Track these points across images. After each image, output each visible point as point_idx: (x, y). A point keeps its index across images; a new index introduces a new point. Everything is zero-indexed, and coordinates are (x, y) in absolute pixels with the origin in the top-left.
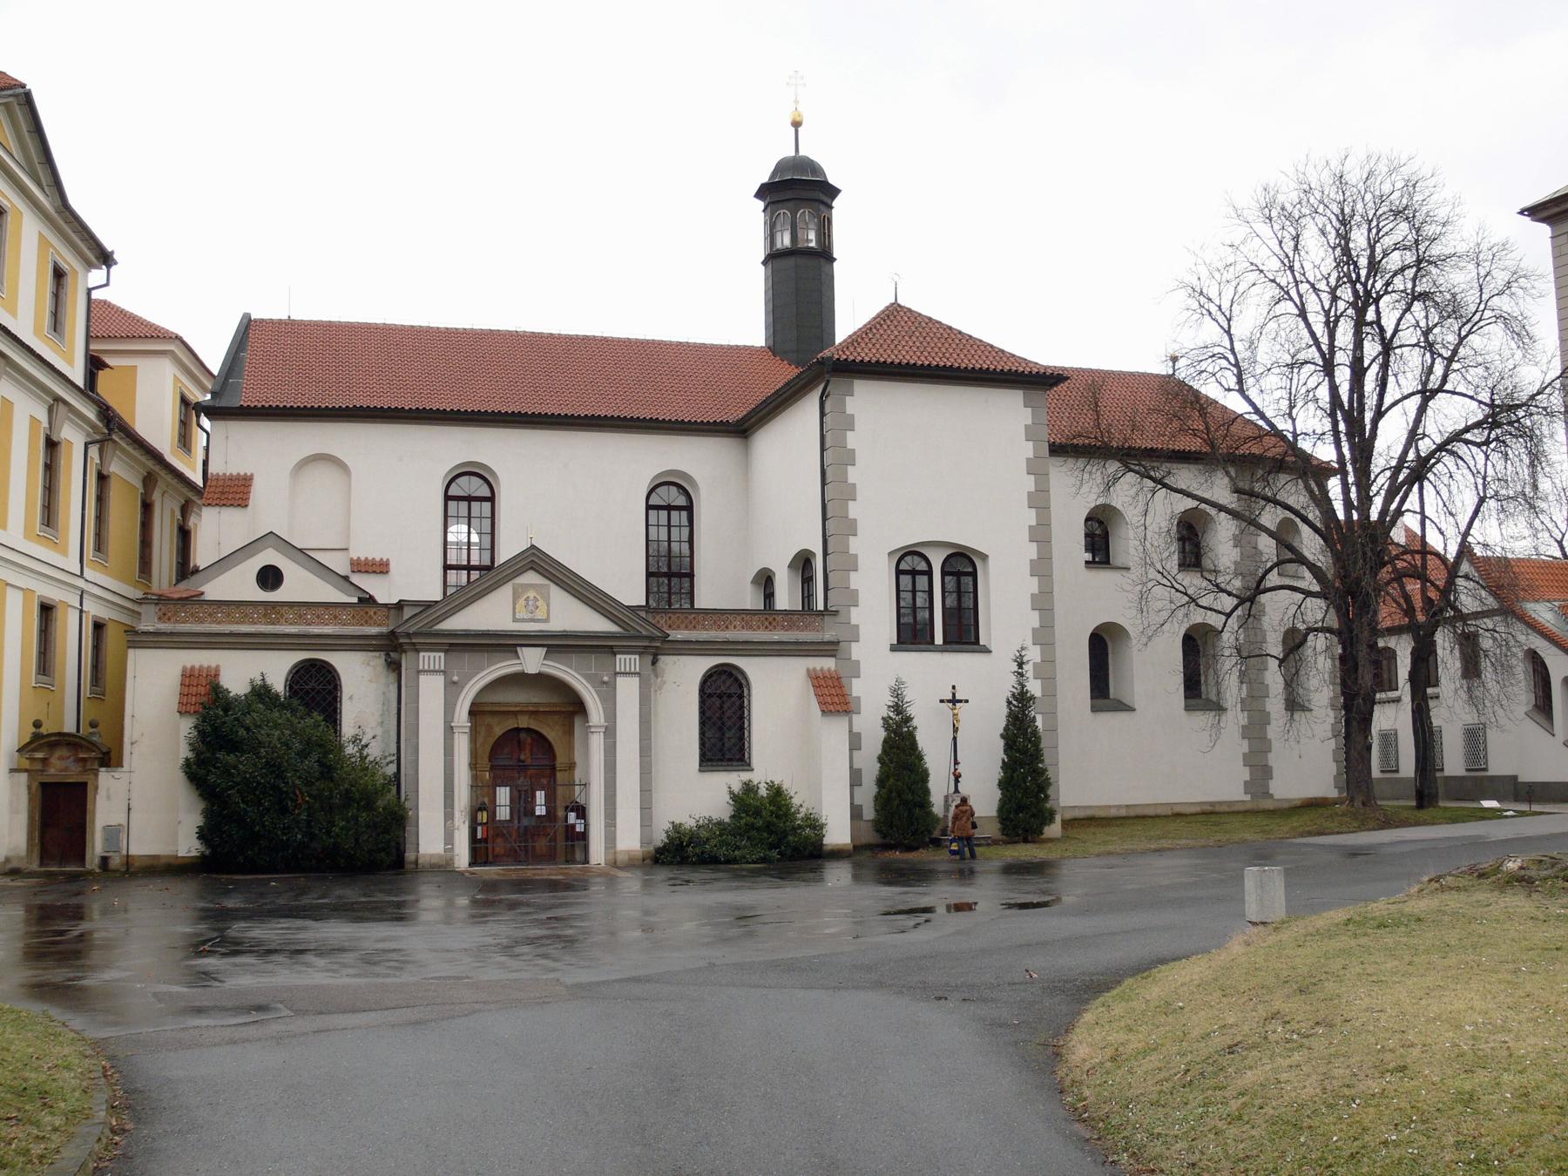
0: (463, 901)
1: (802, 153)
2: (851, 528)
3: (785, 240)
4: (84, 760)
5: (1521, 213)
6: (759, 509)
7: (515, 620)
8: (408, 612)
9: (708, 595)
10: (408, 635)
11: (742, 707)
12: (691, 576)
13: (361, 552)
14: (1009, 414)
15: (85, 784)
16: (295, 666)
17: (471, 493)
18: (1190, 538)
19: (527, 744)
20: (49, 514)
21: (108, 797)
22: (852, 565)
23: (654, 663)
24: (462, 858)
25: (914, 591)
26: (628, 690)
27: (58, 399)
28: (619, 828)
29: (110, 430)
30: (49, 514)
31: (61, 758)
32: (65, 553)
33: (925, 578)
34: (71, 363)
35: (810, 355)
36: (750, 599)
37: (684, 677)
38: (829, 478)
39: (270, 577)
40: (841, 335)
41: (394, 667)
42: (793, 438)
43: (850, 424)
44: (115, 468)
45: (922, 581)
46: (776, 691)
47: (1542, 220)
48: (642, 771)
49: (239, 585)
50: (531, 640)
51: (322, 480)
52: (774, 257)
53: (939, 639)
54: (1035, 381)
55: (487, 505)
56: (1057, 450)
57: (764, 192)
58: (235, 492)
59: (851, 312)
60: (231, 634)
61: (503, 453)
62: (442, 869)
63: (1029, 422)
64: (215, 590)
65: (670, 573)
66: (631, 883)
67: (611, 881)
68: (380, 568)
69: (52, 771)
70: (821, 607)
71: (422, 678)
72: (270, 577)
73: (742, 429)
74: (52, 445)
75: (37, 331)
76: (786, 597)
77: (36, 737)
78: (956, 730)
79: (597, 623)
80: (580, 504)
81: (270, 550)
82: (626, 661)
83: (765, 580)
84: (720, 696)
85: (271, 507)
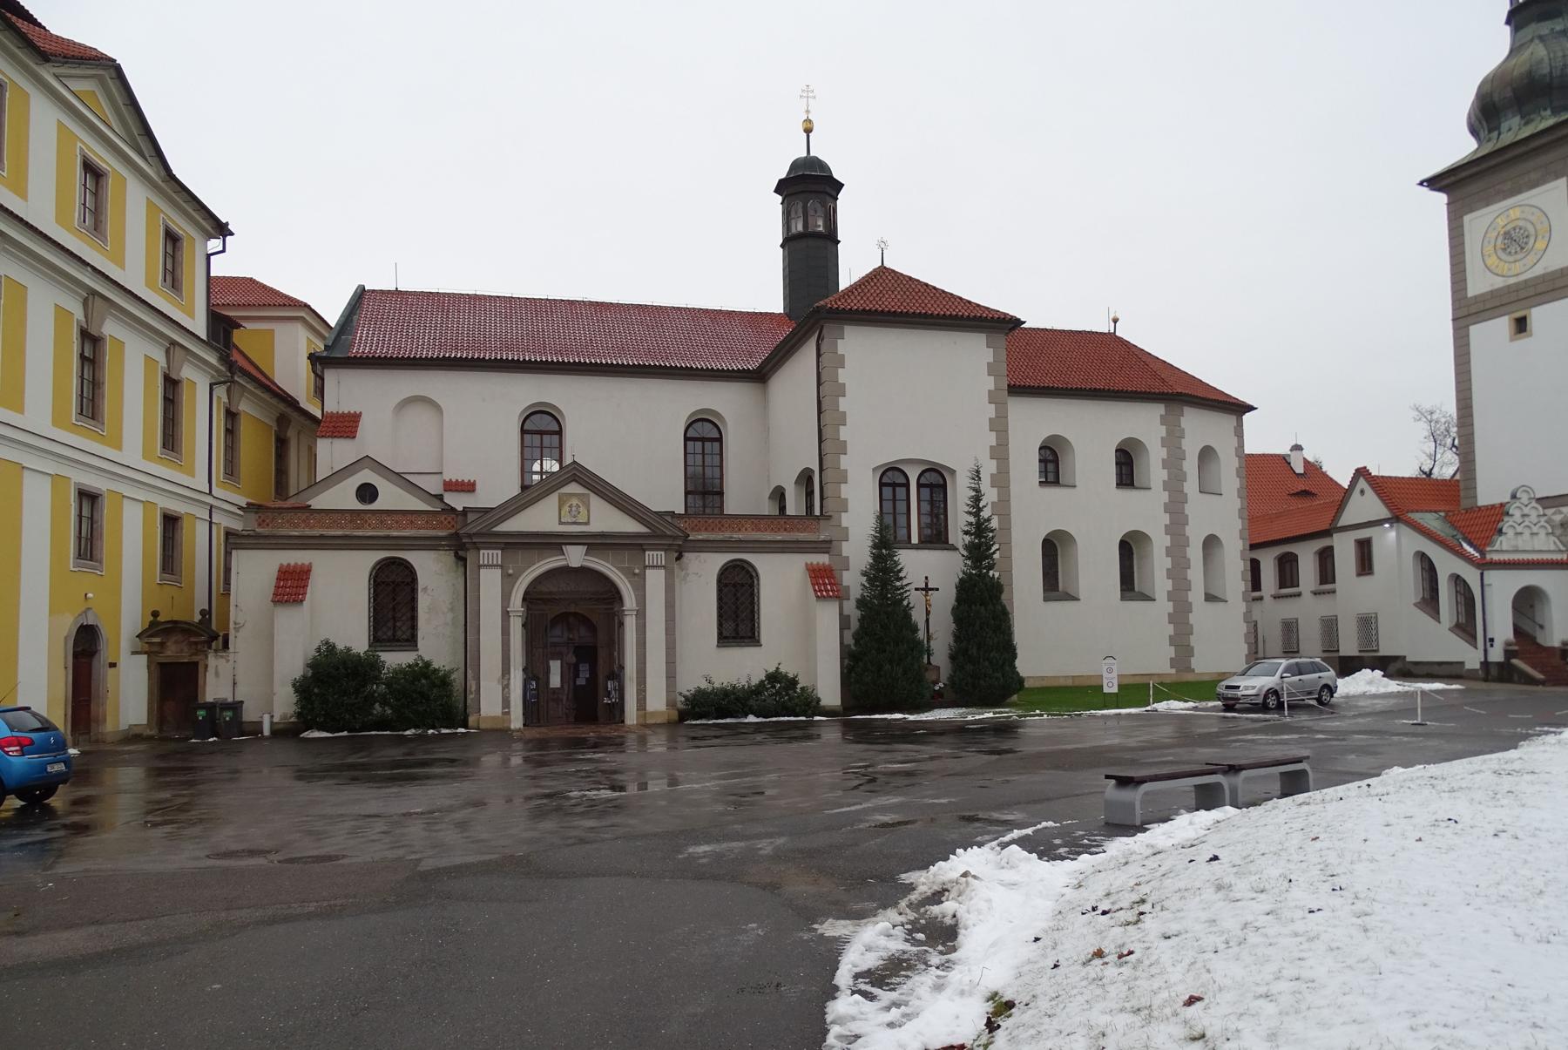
0: (516, 760)
1: (812, 154)
2: (842, 448)
3: (799, 227)
4: (196, 643)
5: (1421, 184)
6: (769, 440)
7: (561, 523)
8: (471, 517)
9: (732, 505)
10: (470, 536)
11: (752, 594)
12: (721, 493)
13: (451, 475)
14: (974, 357)
15: (196, 664)
16: (379, 563)
17: (541, 429)
18: (1127, 466)
19: (576, 627)
20: (171, 438)
21: (217, 674)
23: (679, 558)
24: (516, 721)
25: (894, 500)
26: (655, 580)
27: (174, 343)
28: (649, 690)
29: (233, 374)
30: (171, 438)
31: (176, 642)
32: (192, 474)
34: (191, 315)
35: (823, 301)
36: (767, 508)
37: (705, 570)
39: (367, 493)
40: (844, 284)
41: (461, 560)
42: (796, 380)
44: (244, 407)
45: (901, 492)
46: (780, 580)
47: (1440, 190)
48: (671, 642)
49: (342, 497)
50: (575, 539)
51: (419, 418)
52: (789, 241)
53: (915, 540)
54: (1000, 325)
55: (716, 445)
56: (1016, 390)
57: (781, 188)
58: (345, 426)
59: (852, 267)
60: (322, 536)
61: (573, 399)
62: (499, 735)
64: (320, 502)
65: (704, 489)
66: (658, 745)
67: (643, 741)
68: (469, 487)
69: (169, 653)
70: (817, 512)
71: (482, 571)
72: (367, 493)
73: (760, 376)
74: (172, 385)
75: (149, 284)
76: (794, 506)
77: (152, 624)
78: (928, 613)
79: (630, 526)
80: (630, 438)
81: (366, 471)
82: (653, 556)
83: (779, 495)
84: (734, 586)
85: (374, 439)
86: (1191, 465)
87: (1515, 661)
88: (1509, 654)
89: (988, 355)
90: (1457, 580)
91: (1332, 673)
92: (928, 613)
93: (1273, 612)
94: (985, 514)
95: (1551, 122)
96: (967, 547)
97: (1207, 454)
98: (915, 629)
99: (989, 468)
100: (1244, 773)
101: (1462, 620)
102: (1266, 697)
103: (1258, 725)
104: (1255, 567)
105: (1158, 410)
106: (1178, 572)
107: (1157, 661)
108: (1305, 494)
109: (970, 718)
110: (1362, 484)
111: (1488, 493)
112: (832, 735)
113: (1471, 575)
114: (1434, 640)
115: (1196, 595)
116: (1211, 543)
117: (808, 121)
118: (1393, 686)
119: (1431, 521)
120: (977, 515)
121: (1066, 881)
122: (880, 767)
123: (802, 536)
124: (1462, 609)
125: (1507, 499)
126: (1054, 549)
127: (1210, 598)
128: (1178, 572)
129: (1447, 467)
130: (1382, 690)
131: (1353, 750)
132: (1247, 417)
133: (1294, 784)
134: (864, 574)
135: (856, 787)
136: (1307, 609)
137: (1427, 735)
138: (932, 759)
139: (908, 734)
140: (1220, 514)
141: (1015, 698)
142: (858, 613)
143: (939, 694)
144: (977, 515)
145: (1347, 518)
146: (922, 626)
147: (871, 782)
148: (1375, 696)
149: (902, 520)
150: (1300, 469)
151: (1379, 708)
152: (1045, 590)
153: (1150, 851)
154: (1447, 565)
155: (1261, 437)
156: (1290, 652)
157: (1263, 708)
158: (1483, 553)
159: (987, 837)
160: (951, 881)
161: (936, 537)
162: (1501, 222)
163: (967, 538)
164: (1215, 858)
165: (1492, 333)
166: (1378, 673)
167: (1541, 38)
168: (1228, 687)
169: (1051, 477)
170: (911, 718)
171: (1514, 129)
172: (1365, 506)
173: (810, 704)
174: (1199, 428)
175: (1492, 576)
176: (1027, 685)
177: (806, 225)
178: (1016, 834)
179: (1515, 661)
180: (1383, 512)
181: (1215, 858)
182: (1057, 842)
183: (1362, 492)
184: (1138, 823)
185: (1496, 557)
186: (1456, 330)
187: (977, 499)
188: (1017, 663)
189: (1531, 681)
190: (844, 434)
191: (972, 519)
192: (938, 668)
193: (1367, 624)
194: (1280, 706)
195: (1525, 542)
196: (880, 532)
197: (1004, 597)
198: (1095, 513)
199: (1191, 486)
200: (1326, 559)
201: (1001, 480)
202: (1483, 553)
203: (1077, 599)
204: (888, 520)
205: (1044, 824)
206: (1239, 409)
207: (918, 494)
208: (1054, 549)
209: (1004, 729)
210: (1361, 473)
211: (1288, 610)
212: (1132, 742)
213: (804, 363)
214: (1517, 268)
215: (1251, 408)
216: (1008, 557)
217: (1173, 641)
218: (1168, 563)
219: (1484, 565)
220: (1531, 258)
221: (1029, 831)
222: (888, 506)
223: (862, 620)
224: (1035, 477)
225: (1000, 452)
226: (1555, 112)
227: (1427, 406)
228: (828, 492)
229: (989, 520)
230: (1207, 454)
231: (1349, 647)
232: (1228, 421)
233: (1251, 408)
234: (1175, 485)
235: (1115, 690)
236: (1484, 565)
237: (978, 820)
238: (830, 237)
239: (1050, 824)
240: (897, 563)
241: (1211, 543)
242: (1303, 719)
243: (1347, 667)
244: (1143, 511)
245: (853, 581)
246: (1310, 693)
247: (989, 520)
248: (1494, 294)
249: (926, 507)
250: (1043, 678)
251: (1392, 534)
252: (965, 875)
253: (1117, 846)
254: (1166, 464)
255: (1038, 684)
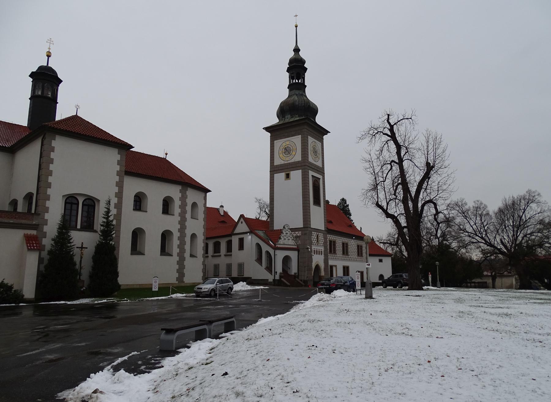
14: (112, 157)
18: (167, 206)
22: (48, 198)
25: (71, 210)
33: (76, 206)
38: (42, 167)
40: (58, 118)
42: (30, 156)
43: (53, 149)
45: (74, 207)
53: (79, 227)
54: (123, 147)
57: (32, 75)
59: (62, 112)
63: (119, 159)
70: (33, 211)
73: (12, 151)
78: (81, 258)
86: (189, 208)
87: (282, 279)
88: (281, 277)
89: (118, 157)
90: (268, 253)
91: (232, 283)
92: (81, 258)
93: (213, 261)
94: (111, 218)
95: (298, 118)
96: (101, 231)
97: (194, 205)
98: (75, 264)
99: (114, 200)
100: (214, 324)
101: (268, 266)
102: (211, 292)
103: (209, 302)
104: (207, 246)
105: (179, 188)
106: (181, 246)
107: (172, 278)
108: (223, 222)
109: (96, 302)
110: (242, 220)
111: (277, 226)
112: (28, 313)
113: (271, 251)
114: (259, 272)
115: (187, 255)
116: (193, 236)
117: (49, 52)
118: (249, 288)
119: (261, 233)
120: (107, 218)
121: (147, 387)
122: (52, 328)
123: (23, 221)
124: (268, 262)
125: (282, 228)
126: (137, 235)
127: (192, 256)
128: (181, 246)
129: (264, 218)
130: (246, 289)
131: (243, 311)
132: (208, 194)
133: (229, 328)
134: (53, 240)
135: (38, 340)
136: (222, 261)
137: (264, 305)
138: (77, 322)
139: (67, 310)
140: (197, 226)
141: (116, 293)
142: (48, 257)
143: (83, 292)
144: (107, 218)
145: (237, 231)
146: (78, 263)
147: (46, 337)
148: (244, 291)
149: (73, 219)
150: (222, 214)
151: (245, 295)
152: (131, 250)
153: (186, 367)
154: (265, 248)
155: (212, 202)
156: (216, 275)
157: (209, 296)
158: (275, 245)
159: (105, 363)
160: (87, 395)
161: (88, 226)
162: (284, 144)
163: (102, 228)
164: (226, 374)
165: (280, 177)
166: (245, 283)
167: (296, 94)
168: (198, 288)
169: (138, 208)
170: (69, 303)
171: (288, 119)
172: (242, 227)
173: (18, 297)
174: (192, 196)
175: (278, 252)
176: (122, 288)
177: (42, 92)
178: (120, 360)
179: (282, 279)
180: (247, 229)
181: (226, 374)
182: (140, 362)
183: (242, 223)
184: (174, 349)
185: (279, 246)
186: (270, 174)
187: (108, 212)
188: (118, 279)
189: (286, 285)
190: (50, 179)
191: (105, 220)
192: (83, 281)
193: (241, 266)
194: (215, 295)
195: (286, 242)
196: (63, 222)
197: (115, 252)
198: (153, 222)
199: (188, 215)
200: (229, 243)
201: (119, 206)
202: (275, 245)
203: (144, 254)
204: (67, 218)
205: (133, 353)
206: (206, 191)
207: (82, 209)
208: (137, 235)
209: (111, 307)
210: (242, 216)
211: (216, 261)
212: (164, 311)
213: (35, 148)
214: (287, 159)
215: (210, 191)
216: (118, 237)
217: (178, 271)
218: (178, 242)
219: (275, 248)
220: (291, 157)
221: (126, 358)
222: (68, 212)
223: (49, 260)
224: (132, 207)
225: (119, 195)
226: (299, 116)
227: (259, 198)
228: (40, 203)
229: (112, 221)
230: (194, 205)
231: (235, 274)
232: (202, 195)
233: (210, 191)
234: (183, 215)
235: (157, 290)
236: (275, 248)
237: (101, 353)
238: (54, 100)
239: (136, 353)
240: (69, 236)
241: (193, 236)
242: (223, 299)
243: (236, 281)
244: (171, 223)
245: (47, 242)
246: (225, 290)
247: (112, 221)
248: (281, 165)
249: (85, 214)
250: (127, 285)
251: (250, 237)
252: (95, 392)
253: (168, 362)
254: (180, 207)
255: (126, 287)
